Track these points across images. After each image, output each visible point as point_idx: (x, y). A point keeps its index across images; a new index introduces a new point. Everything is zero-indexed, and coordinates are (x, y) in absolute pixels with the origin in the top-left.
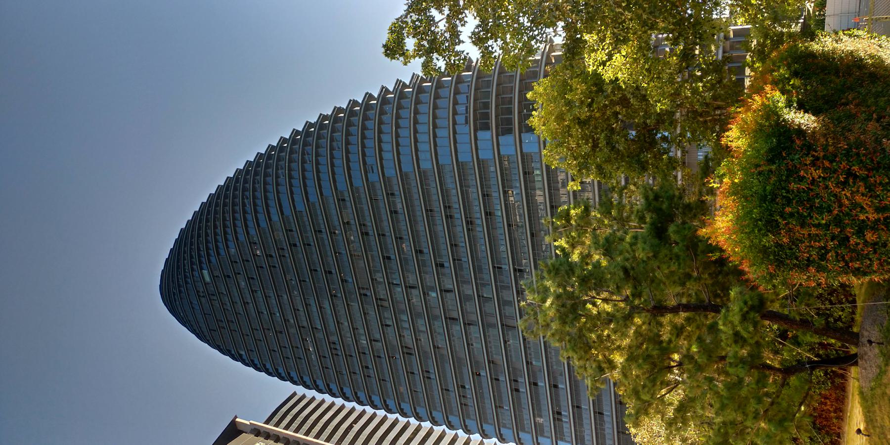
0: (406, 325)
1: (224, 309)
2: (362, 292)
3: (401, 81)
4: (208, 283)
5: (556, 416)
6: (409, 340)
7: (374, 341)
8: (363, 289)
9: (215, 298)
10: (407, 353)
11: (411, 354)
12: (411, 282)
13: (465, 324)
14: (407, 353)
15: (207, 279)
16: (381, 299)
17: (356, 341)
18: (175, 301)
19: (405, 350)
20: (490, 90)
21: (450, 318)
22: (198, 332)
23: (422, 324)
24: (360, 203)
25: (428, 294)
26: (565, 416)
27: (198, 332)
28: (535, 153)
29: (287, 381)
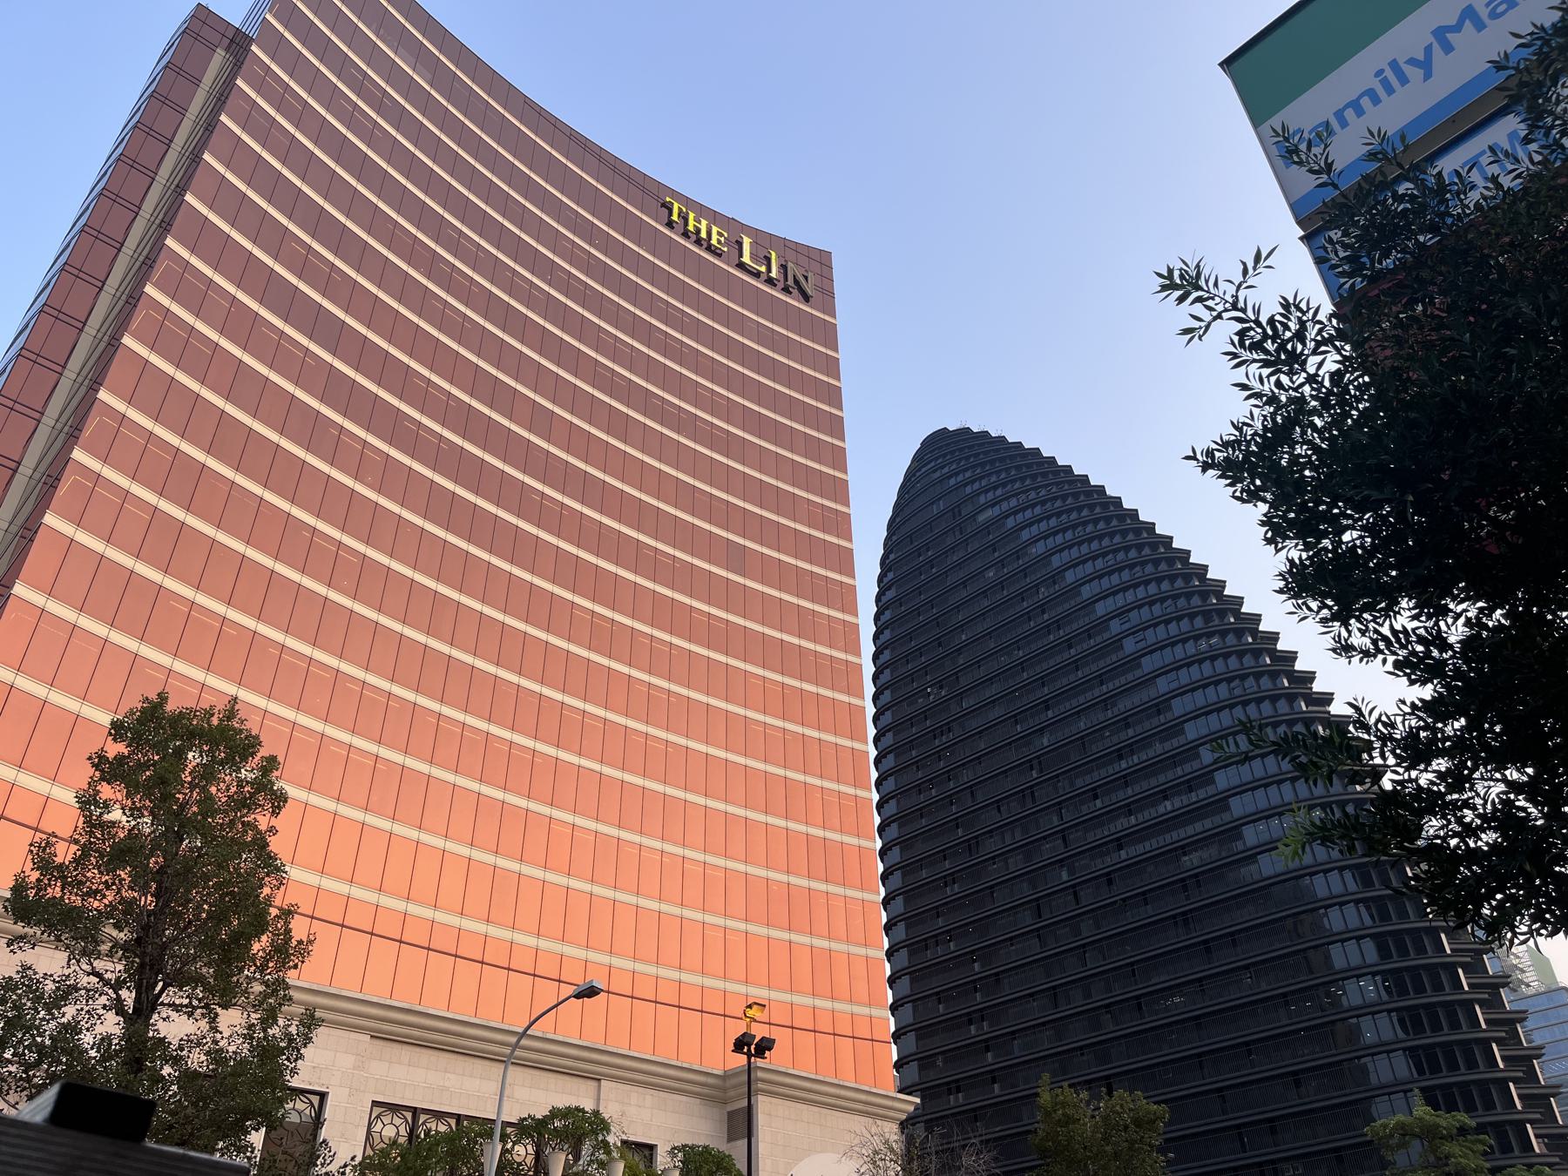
0: (1008, 840)
1: (946, 552)
2: (1035, 762)
3: (1260, 620)
4: (975, 520)
5: (953, 1085)
6: (991, 846)
7: (972, 792)
8: (1040, 763)
9: (957, 533)
10: (969, 845)
11: (970, 850)
12: (1071, 837)
13: (1038, 929)
14: (969, 845)
15: (981, 518)
16: (1032, 793)
17: (963, 764)
18: (930, 452)
19: (956, 510)
20: (1395, 958)
21: (1038, 906)
22: (898, 520)
23: (1016, 864)
24: (1162, 741)
25: (1062, 866)
26: (957, 1098)
27: (898, 520)
28: (1244, 843)
29: (876, 624)
